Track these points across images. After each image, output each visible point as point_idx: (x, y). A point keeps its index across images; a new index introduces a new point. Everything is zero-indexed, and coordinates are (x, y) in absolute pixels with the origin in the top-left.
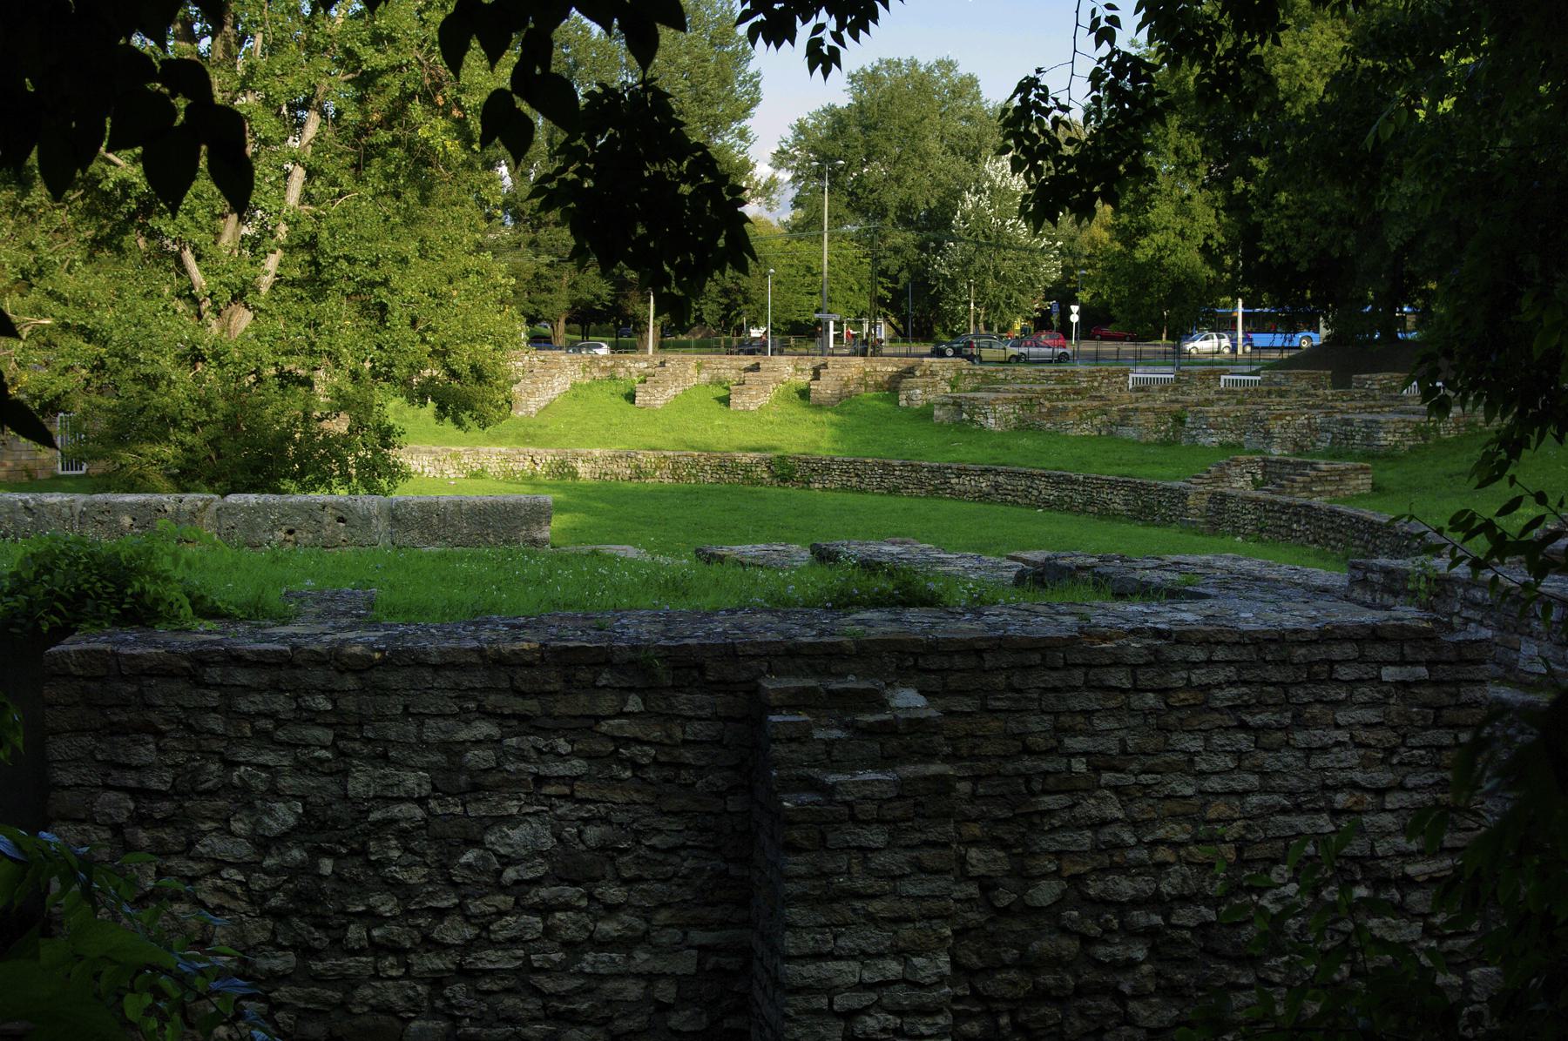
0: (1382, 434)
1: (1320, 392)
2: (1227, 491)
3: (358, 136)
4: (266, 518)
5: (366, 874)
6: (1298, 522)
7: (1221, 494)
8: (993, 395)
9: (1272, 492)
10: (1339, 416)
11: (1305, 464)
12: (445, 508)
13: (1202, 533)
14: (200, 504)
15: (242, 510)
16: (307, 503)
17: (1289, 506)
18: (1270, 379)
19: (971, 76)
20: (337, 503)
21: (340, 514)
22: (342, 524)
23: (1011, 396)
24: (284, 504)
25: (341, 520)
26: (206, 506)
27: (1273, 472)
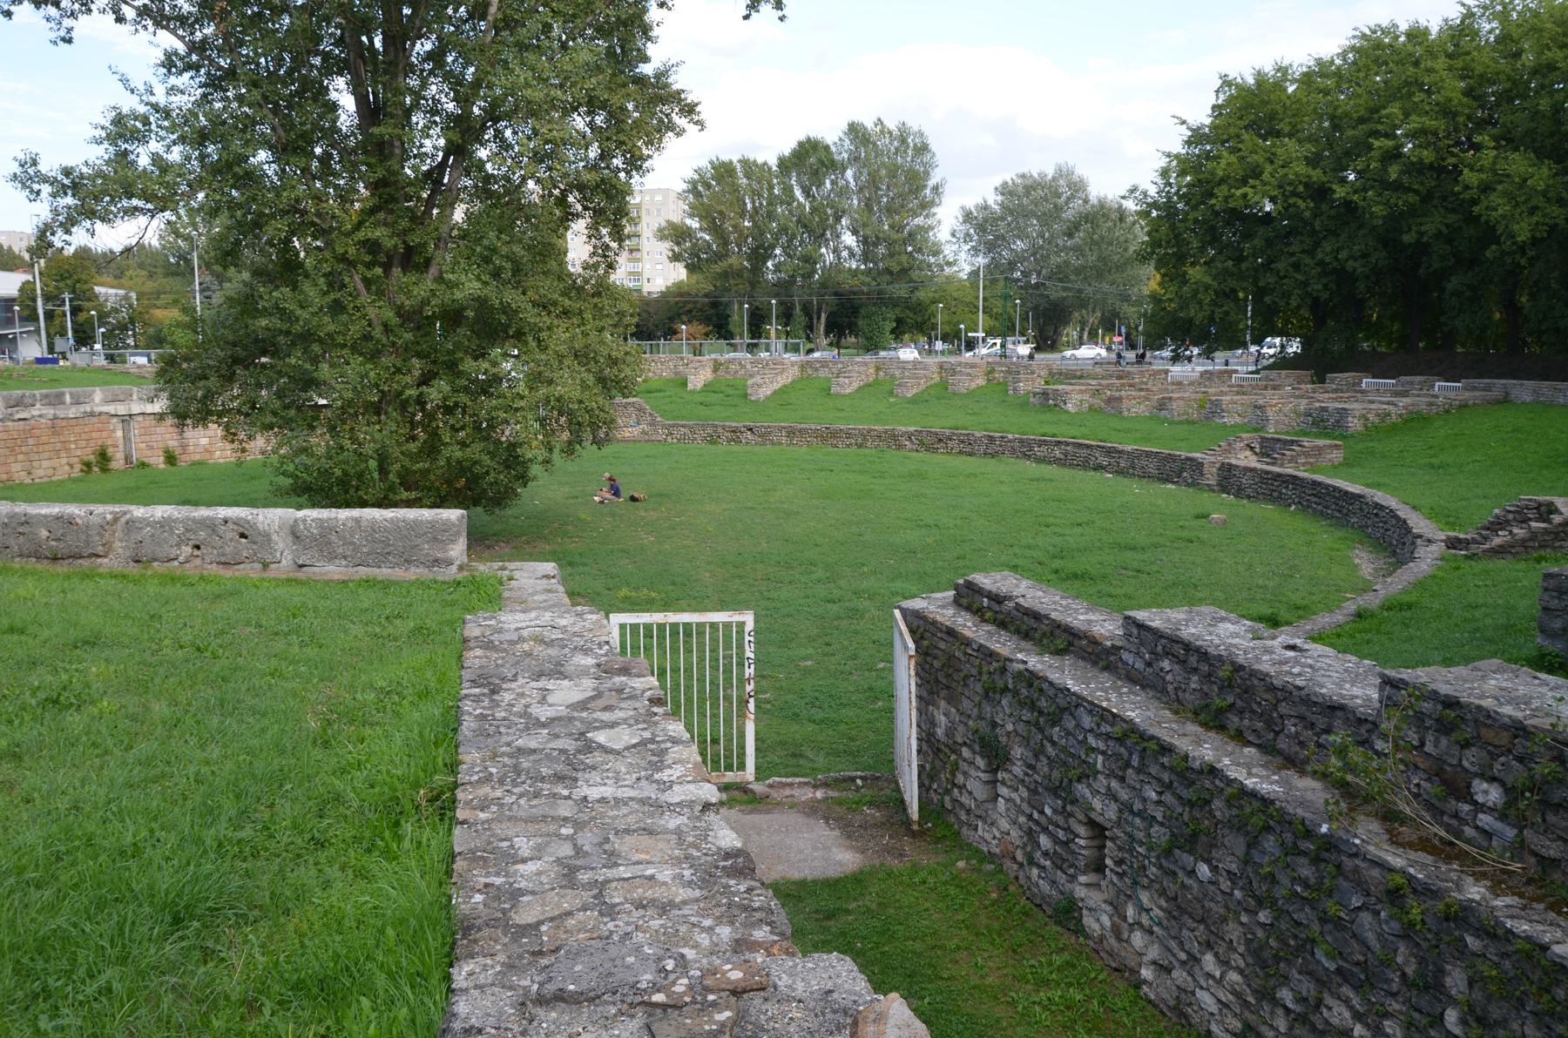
0: (1350, 419)
1: (1303, 386)
2: (1234, 462)
3: (549, 156)
4: (172, 533)
5: (1043, 662)
6: (1287, 488)
7: (1229, 464)
8: (1071, 387)
9: (1268, 464)
10: (1317, 405)
11: (1292, 442)
12: (344, 524)
13: (1213, 491)
14: (109, 517)
15: (148, 524)
16: (208, 518)
17: (1279, 475)
18: (1267, 376)
19: (809, 140)
20: (237, 518)
21: (241, 530)
22: (243, 540)
23: (1083, 388)
24: (188, 519)
25: (243, 536)
26: (116, 520)
27: (1268, 448)
